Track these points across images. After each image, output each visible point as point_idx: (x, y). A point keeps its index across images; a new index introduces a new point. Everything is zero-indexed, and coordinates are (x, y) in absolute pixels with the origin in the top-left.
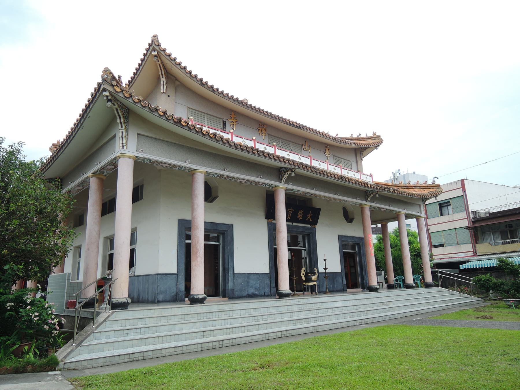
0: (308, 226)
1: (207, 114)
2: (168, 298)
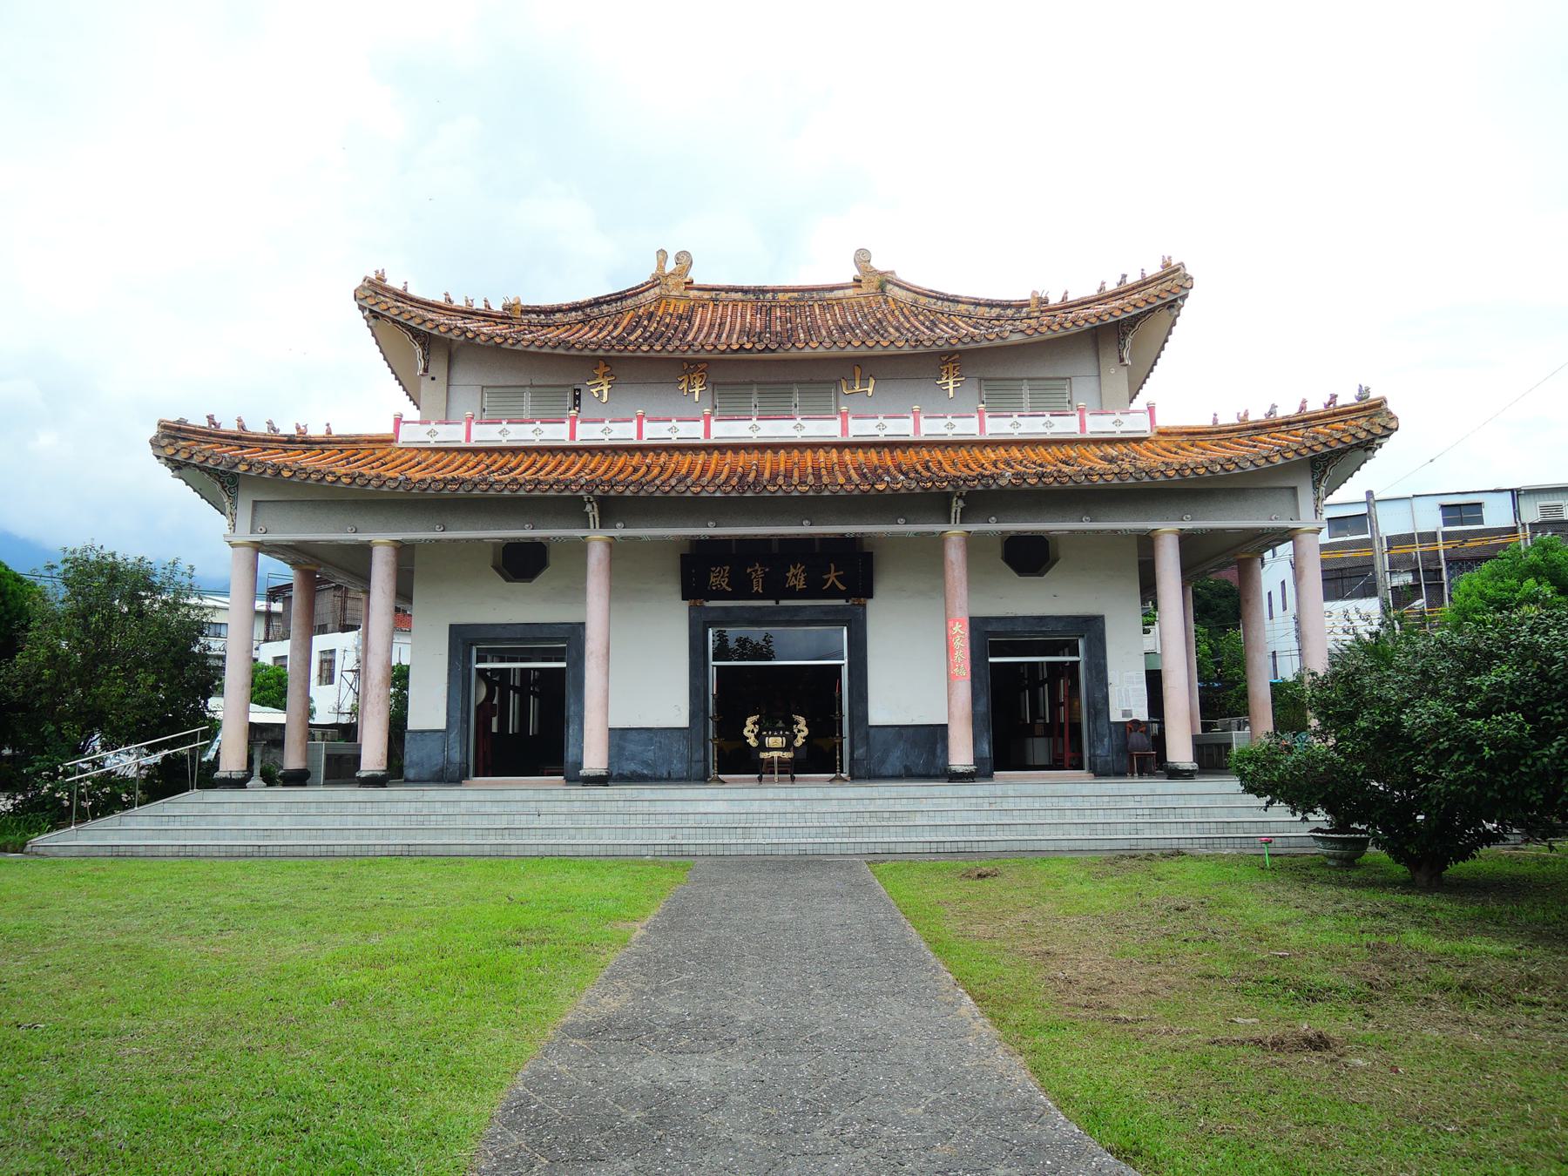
0: (842, 602)
1: (532, 386)
2: (426, 775)
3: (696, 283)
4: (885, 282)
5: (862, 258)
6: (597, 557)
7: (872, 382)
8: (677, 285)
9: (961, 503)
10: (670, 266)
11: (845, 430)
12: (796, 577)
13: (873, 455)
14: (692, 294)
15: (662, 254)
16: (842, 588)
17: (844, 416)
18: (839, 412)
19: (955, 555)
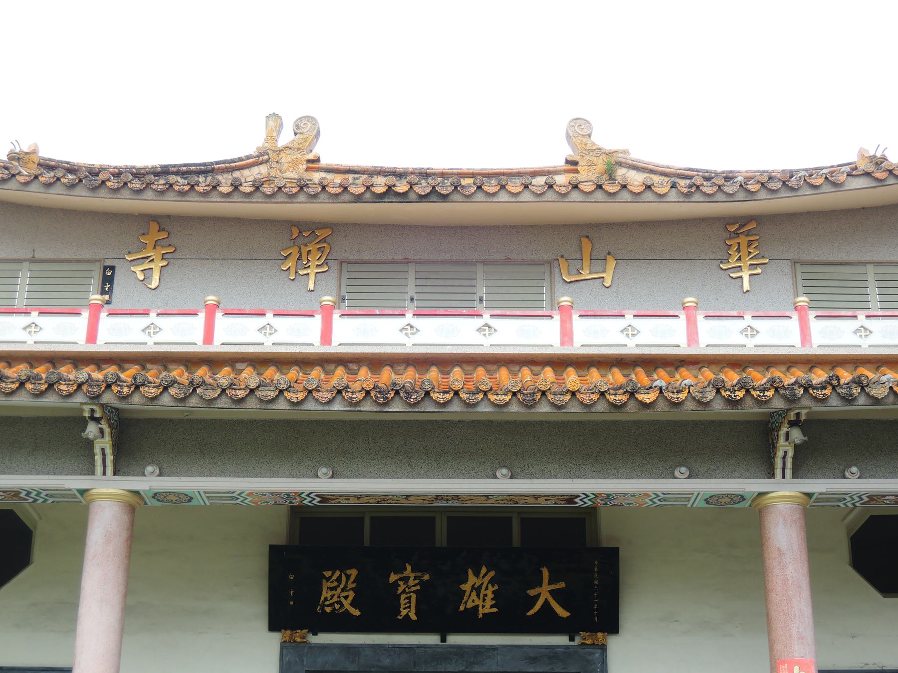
0: (561, 640)
1: (33, 260)
3: (324, 162)
4: (614, 164)
5: (578, 131)
6: (105, 529)
7: (611, 264)
8: (295, 163)
9: (797, 435)
10: (286, 138)
11: (566, 335)
12: (479, 592)
13: (617, 376)
14: (317, 177)
15: (275, 119)
16: (562, 613)
17: (566, 312)
18: (553, 303)
19: (785, 538)
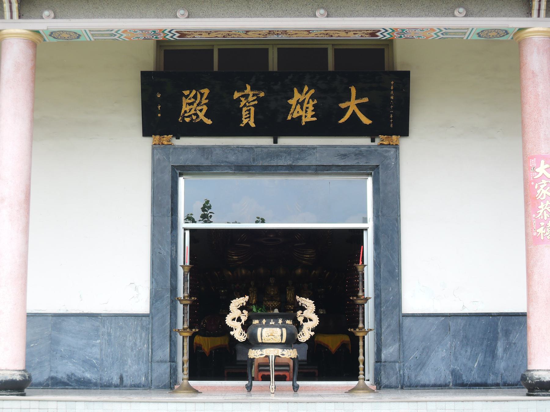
0: (365, 141)
16: (366, 121)
